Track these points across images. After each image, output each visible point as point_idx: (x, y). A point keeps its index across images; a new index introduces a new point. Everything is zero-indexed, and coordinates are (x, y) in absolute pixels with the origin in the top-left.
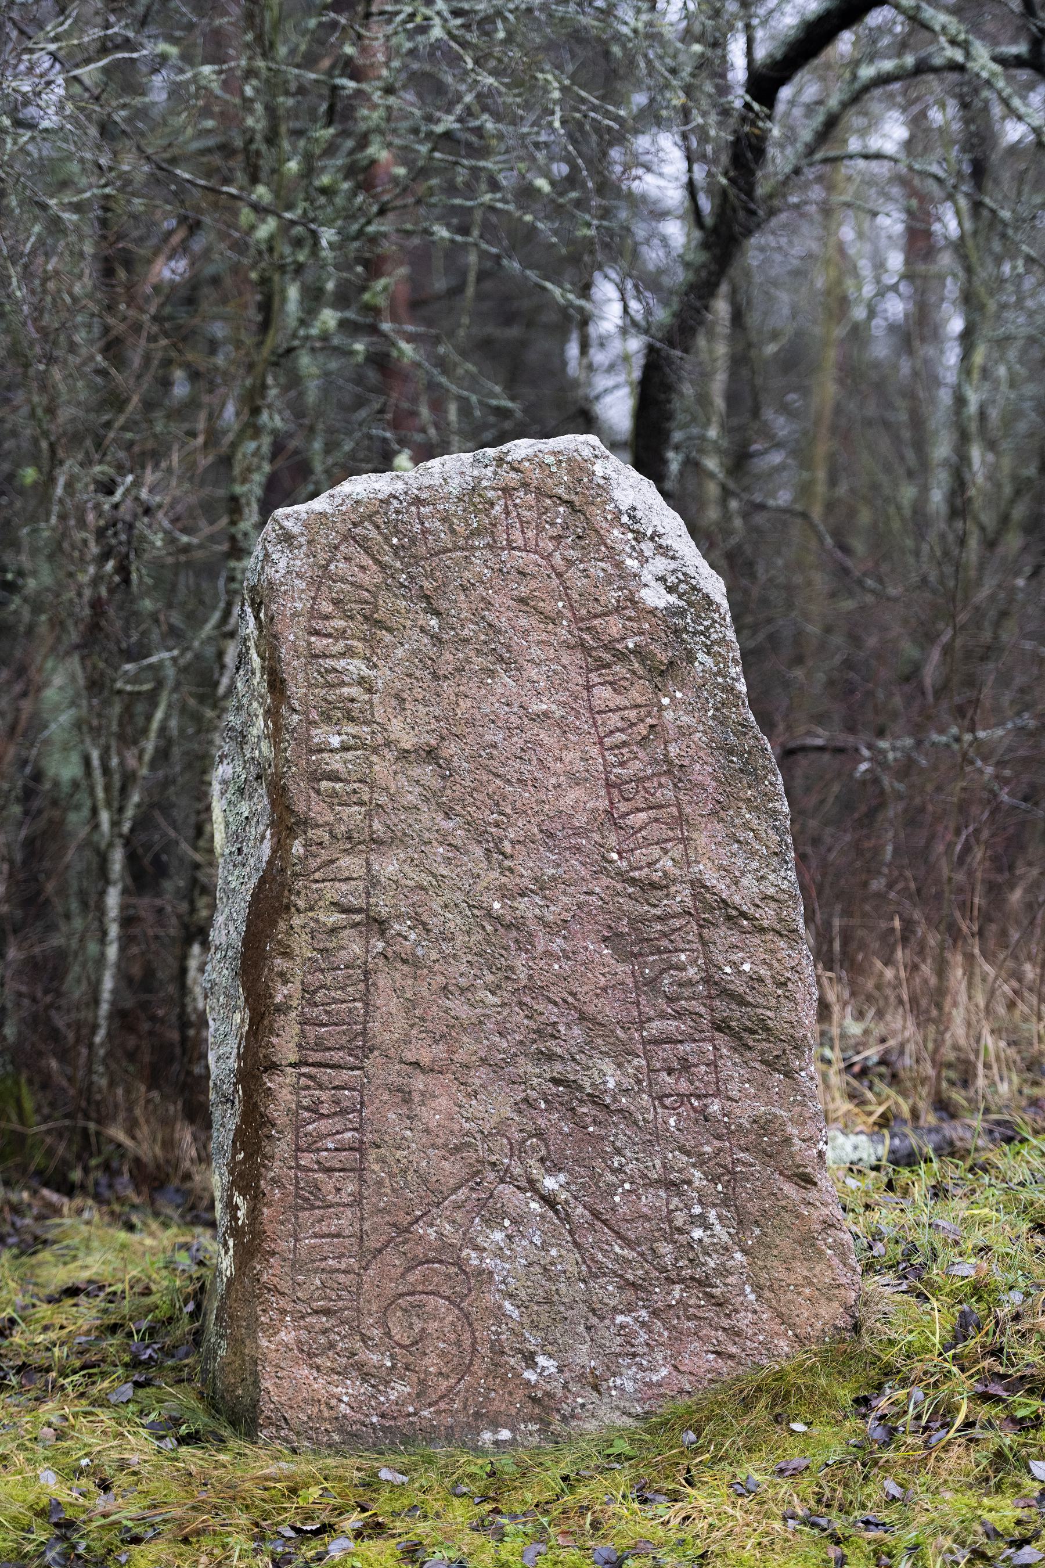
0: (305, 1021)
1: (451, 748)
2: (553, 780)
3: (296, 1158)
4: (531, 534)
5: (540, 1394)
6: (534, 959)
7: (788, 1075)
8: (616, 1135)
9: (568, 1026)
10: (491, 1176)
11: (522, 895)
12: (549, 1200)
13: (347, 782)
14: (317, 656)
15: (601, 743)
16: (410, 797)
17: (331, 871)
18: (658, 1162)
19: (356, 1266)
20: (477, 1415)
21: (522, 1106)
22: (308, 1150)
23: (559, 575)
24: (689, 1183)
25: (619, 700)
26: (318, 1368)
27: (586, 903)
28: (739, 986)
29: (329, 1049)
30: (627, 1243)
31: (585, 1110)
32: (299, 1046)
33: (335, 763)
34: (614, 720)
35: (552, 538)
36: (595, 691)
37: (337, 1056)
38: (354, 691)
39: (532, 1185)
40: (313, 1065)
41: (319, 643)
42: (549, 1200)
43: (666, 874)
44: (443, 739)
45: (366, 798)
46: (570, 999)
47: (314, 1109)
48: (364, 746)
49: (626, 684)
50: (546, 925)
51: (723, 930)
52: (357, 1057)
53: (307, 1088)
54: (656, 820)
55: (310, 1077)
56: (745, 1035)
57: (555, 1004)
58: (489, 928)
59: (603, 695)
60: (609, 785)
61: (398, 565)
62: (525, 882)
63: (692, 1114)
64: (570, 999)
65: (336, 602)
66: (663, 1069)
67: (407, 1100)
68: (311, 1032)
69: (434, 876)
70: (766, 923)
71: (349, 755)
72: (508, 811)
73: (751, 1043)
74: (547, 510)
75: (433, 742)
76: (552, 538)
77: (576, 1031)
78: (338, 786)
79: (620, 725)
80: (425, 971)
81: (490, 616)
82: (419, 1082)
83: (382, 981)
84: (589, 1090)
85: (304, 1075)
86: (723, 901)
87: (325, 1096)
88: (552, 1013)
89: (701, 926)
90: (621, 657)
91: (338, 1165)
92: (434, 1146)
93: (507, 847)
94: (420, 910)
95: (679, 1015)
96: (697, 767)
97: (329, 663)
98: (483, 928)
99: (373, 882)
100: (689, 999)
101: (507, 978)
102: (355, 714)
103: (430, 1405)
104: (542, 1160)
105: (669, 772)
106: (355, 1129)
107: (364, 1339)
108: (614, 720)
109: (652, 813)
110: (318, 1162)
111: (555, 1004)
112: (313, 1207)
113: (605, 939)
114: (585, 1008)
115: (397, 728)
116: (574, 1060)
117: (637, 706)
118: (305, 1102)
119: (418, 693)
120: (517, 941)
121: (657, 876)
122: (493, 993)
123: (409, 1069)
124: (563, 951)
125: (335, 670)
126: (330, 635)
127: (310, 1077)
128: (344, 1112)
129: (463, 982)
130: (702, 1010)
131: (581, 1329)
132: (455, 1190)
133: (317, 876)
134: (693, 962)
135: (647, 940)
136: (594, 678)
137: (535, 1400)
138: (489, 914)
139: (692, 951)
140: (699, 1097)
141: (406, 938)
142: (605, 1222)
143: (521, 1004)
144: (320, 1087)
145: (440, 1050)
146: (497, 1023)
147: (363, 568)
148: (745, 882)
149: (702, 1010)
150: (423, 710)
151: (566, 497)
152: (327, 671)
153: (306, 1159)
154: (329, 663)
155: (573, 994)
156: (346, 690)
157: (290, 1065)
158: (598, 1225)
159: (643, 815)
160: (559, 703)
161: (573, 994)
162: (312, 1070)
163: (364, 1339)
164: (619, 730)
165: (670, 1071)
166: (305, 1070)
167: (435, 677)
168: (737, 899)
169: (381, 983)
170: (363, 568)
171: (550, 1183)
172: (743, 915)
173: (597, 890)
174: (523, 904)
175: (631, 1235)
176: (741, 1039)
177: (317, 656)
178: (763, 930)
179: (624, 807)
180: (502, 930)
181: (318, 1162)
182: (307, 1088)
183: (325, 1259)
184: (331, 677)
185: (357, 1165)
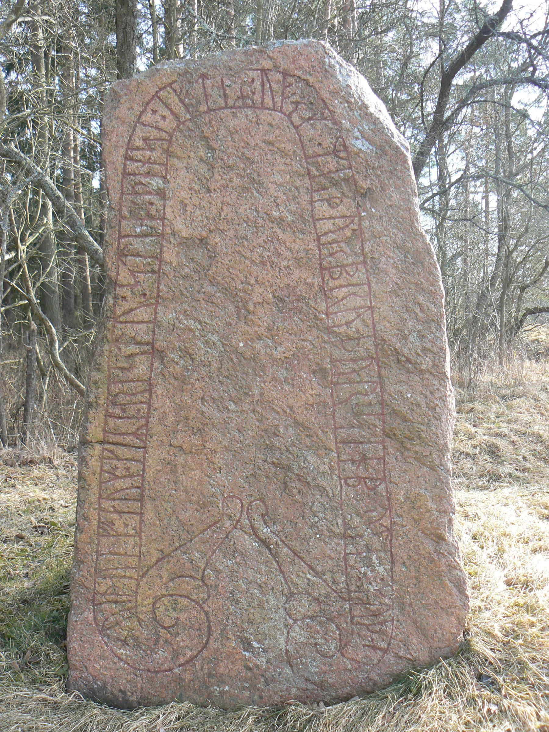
0: (108, 415)
1: (216, 238)
2: (284, 263)
3: (100, 504)
4: (278, 99)
5: (251, 665)
6: (265, 382)
7: (432, 468)
8: (313, 503)
9: (286, 429)
10: (228, 523)
11: (260, 339)
12: (265, 543)
13: (145, 257)
14: (129, 174)
15: (318, 239)
16: (187, 270)
17: (129, 317)
18: (340, 521)
19: (136, 576)
20: (210, 675)
21: (252, 479)
22: (108, 499)
23: (296, 128)
24: (361, 536)
25: (334, 212)
26: (108, 637)
27: (303, 347)
28: (403, 409)
29: (123, 434)
30: (317, 574)
31: (293, 485)
32: (104, 430)
33: (137, 244)
34: (328, 225)
35: (292, 103)
36: (317, 204)
37: (128, 439)
38: (155, 199)
39: (255, 532)
40: (113, 443)
41: (132, 166)
42: (265, 543)
43: (358, 331)
44: (211, 231)
45: (156, 268)
46: (288, 411)
47: (112, 472)
48: (158, 235)
49: (338, 201)
50: (274, 360)
51: (395, 370)
52: (141, 440)
53: (109, 458)
54: (354, 294)
55: (112, 452)
56: (405, 440)
57: (278, 413)
58: (235, 359)
59: (322, 209)
60: (322, 268)
61: (188, 116)
62: (262, 330)
63: (366, 490)
64: (288, 411)
65: (145, 140)
66: (349, 460)
67: (174, 471)
68: (111, 422)
69: (200, 323)
70: (424, 367)
71: (147, 240)
72: (252, 281)
73: (409, 446)
74: (290, 85)
75: (204, 233)
76: (292, 103)
77: (291, 431)
78: (138, 259)
79: (331, 228)
80: (190, 386)
81: (247, 153)
82: (181, 460)
83: (159, 390)
84: (296, 472)
85: (106, 449)
86: (396, 350)
87: (119, 464)
88: (272, 418)
89: (379, 367)
90: (335, 184)
91: (126, 510)
92: (191, 502)
93: (251, 307)
94: (188, 345)
95: (361, 426)
96: (383, 260)
97: (138, 178)
98: (232, 359)
99: (156, 323)
100: (369, 415)
101: (246, 394)
102: (154, 213)
103: (180, 666)
104: (263, 516)
105: (365, 262)
106: (138, 487)
107: (140, 621)
108: (328, 225)
109: (352, 289)
110: (113, 507)
111: (278, 413)
112: (109, 535)
113: (314, 372)
114: (298, 417)
115: (179, 225)
116: (288, 450)
117: (343, 217)
118: (106, 468)
119: (196, 201)
120: (254, 370)
121: (352, 332)
122: (236, 404)
123: (176, 450)
124: (285, 378)
125: (141, 183)
126: (140, 161)
127: (112, 452)
128: (131, 476)
129: (215, 395)
130: (377, 423)
131: (281, 626)
132: (203, 532)
133: (121, 319)
134: (373, 391)
135: (343, 374)
136: (316, 197)
137: (249, 669)
138: (236, 351)
139: (373, 382)
140: (371, 479)
141: (177, 363)
142: (301, 558)
143: (254, 411)
144: (117, 458)
145: (196, 440)
146: (237, 424)
147: (164, 118)
148: (411, 338)
149: (377, 423)
150: (198, 212)
151: (303, 77)
152: (136, 184)
153: (106, 504)
154: (138, 178)
155: (291, 408)
156: (147, 198)
157: (97, 442)
158: (297, 560)
159: (345, 290)
160: (291, 213)
161: (291, 408)
162: (112, 447)
163: (140, 621)
164: (330, 231)
165: (353, 462)
166: (108, 446)
167: (208, 190)
168: (405, 350)
169: (159, 392)
170: (164, 118)
171: (265, 531)
172: (408, 360)
173: (310, 338)
174: (258, 346)
175: (319, 569)
176: (402, 443)
177: (129, 174)
178: (421, 371)
179: (332, 283)
180: (244, 362)
181: (113, 507)
182: (109, 458)
183: (117, 568)
184: (138, 188)
185: (138, 511)
